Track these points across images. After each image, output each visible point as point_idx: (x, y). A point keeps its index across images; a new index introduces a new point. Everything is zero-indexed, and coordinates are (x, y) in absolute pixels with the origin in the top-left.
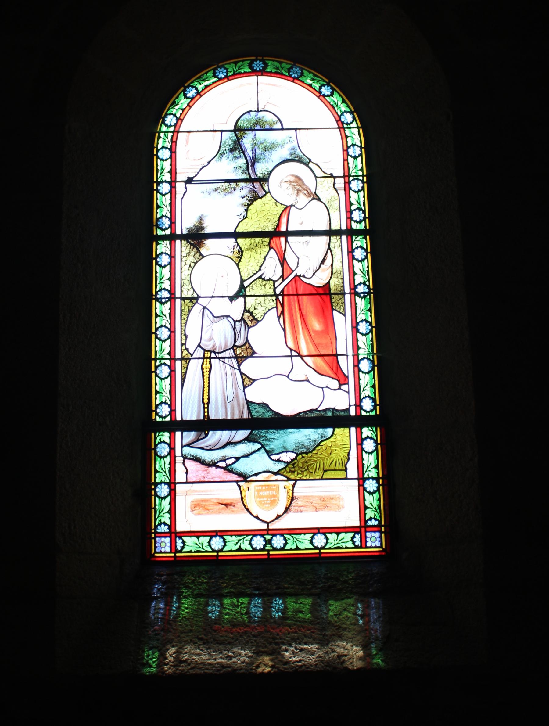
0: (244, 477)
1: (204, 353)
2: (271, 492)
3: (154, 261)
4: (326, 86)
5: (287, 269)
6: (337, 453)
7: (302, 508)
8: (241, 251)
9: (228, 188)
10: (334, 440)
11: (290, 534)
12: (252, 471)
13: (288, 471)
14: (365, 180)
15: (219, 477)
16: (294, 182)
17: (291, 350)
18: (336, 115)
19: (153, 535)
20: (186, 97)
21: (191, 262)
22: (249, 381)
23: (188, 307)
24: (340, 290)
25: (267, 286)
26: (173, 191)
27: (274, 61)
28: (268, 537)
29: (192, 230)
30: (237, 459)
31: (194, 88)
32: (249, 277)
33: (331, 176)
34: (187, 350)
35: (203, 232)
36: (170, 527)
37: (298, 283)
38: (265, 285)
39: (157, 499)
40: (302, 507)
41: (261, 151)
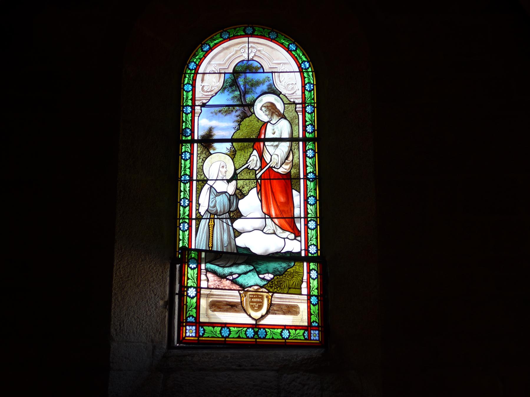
0: (243, 287)
1: (210, 215)
2: (258, 299)
3: (180, 156)
4: (293, 44)
5: (263, 163)
6: (296, 277)
7: (276, 312)
8: (235, 151)
9: (228, 110)
10: (295, 269)
11: (269, 328)
12: (248, 284)
13: (269, 286)
14: (315, 106)
15: (228, 287)
16: (270, 107)
17: (265, 214)
18: (298, 64)
19: (184, 324)
20: (202, 51)
21: (203, 157)
22: (238, 234)
23: (201, 186)
24: (297, 176)
25: (251, 174)
26: (193, 112)
27: (259, 27)
28: (256, 330)
29: (204, 137)
30: (240, 275)
31: (208, 45)
32: (240, 167)
33: (294, 103)
34: (200, 213)
35: (211, 138)
36: (196, 319)
37: (271, 172)
38: (249, 173)
39: (188, 298)
40: (276, 311)
41: (249, 86)
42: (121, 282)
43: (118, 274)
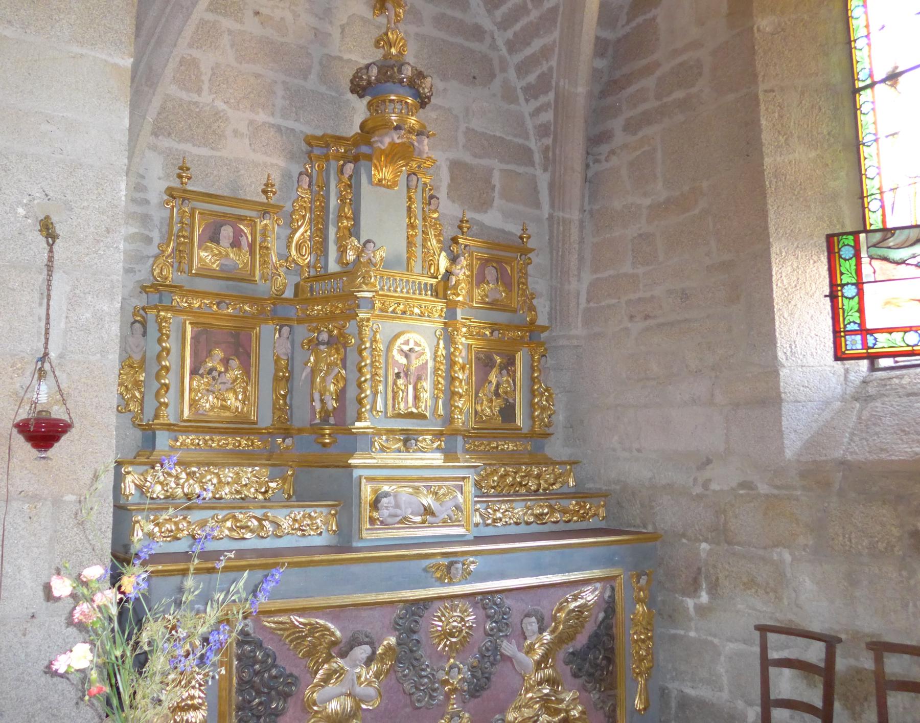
36: (860, 325)
42: (786, 294)
43: (779, 284)
